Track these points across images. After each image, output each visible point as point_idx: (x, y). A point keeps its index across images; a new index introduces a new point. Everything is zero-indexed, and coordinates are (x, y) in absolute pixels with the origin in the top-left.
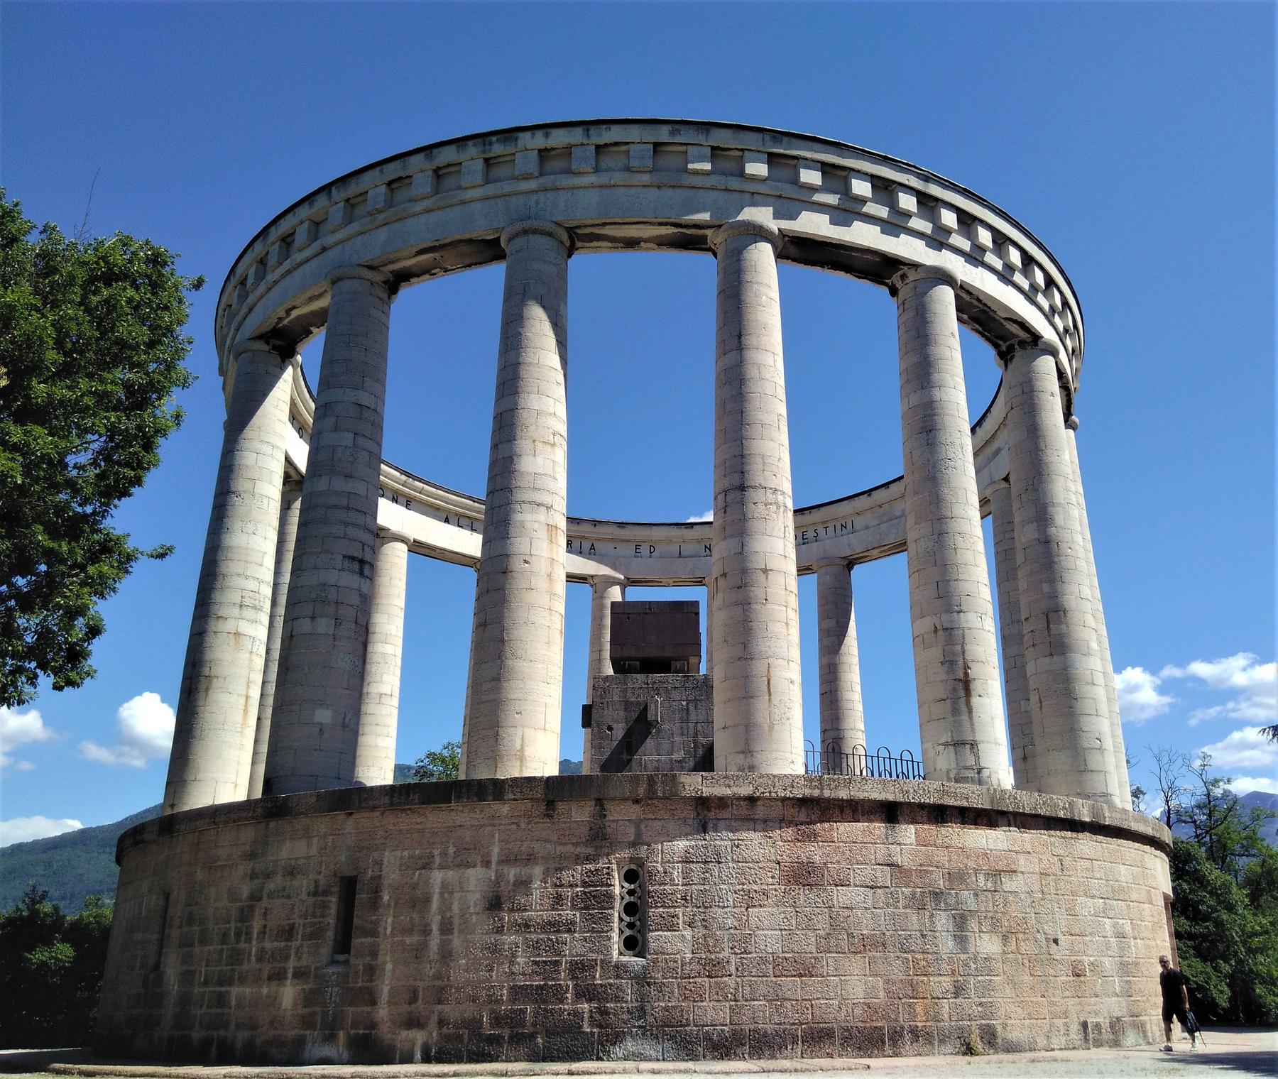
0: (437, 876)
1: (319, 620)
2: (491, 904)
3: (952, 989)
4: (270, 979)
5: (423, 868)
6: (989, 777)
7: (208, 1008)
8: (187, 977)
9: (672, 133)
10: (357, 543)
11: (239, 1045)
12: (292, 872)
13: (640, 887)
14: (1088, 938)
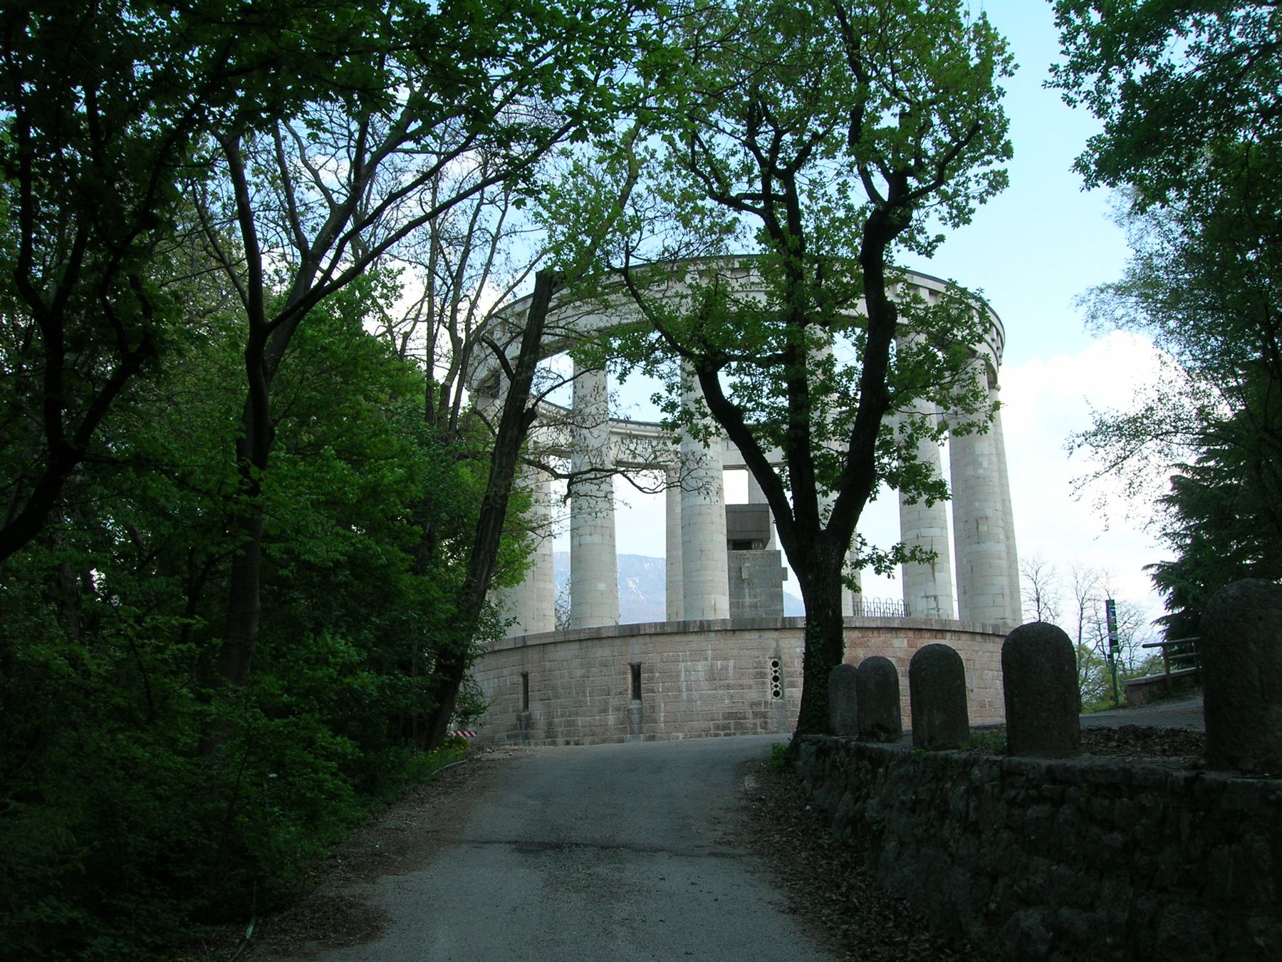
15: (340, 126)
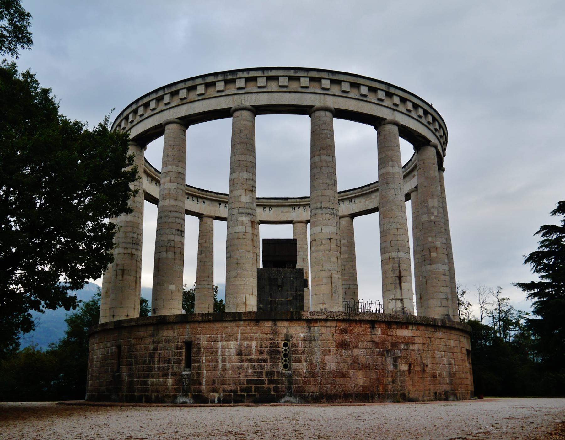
0: (220, 344)
2: (238, 353)
3: (391, 381)
4: (163, 376)
6: (407, 311)
8: (131, 376)
9: (295, 73)
10: (179, 224)
11: (153, 397)
12: (168, 341)
13: (288, 348)
14: (438, 365)
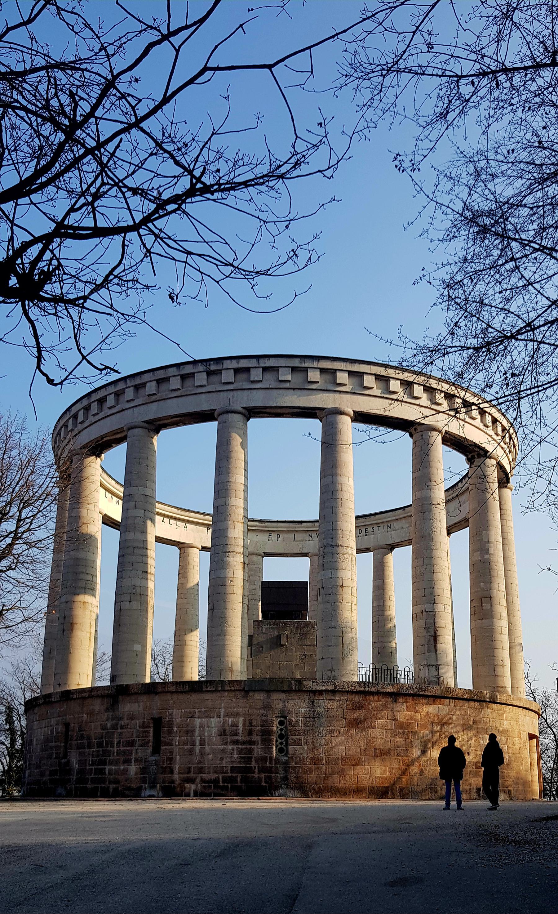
1: (132, 603)
3: (419, 772)
5: (191, 717)
7: (94, 775)
9: (301, 362)
15: (123, 276)
